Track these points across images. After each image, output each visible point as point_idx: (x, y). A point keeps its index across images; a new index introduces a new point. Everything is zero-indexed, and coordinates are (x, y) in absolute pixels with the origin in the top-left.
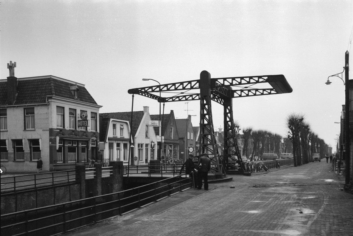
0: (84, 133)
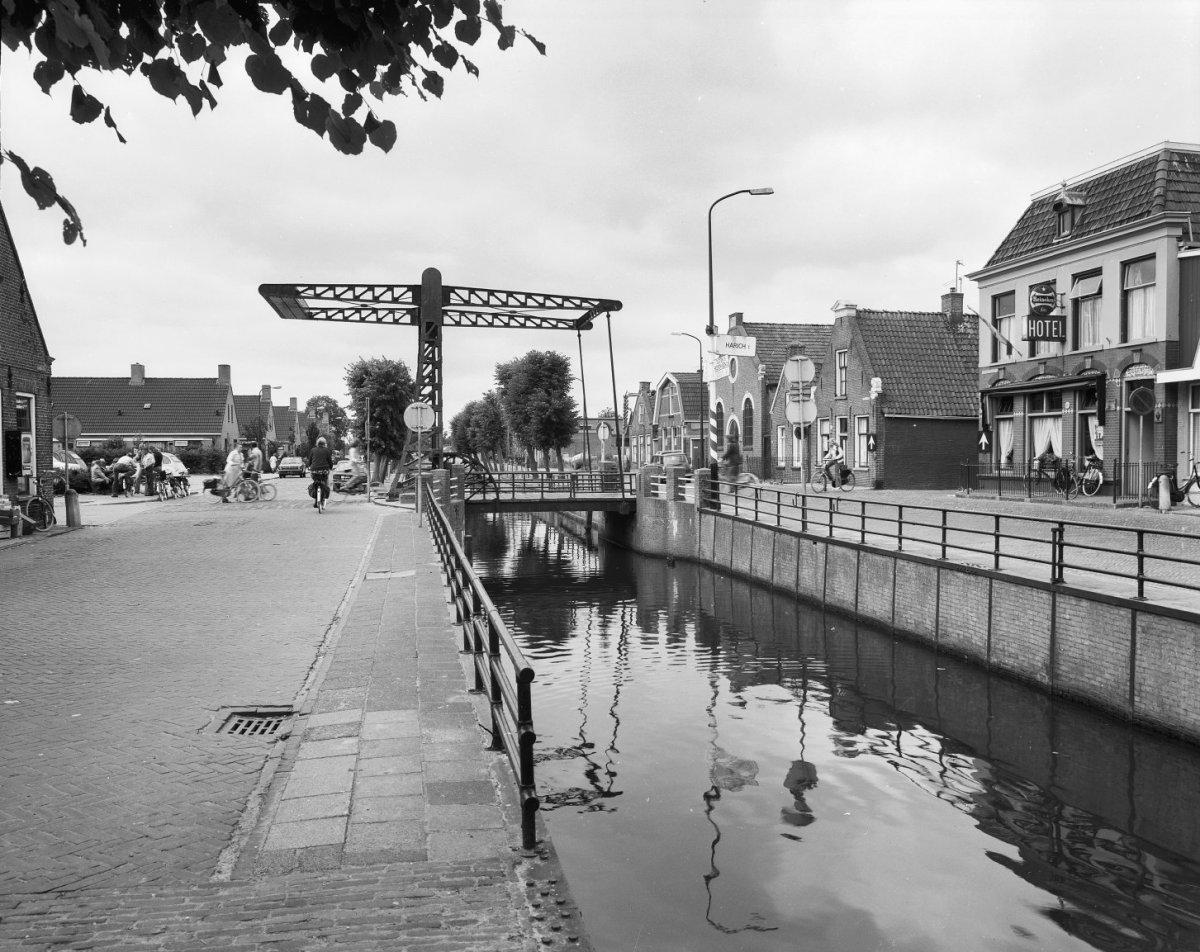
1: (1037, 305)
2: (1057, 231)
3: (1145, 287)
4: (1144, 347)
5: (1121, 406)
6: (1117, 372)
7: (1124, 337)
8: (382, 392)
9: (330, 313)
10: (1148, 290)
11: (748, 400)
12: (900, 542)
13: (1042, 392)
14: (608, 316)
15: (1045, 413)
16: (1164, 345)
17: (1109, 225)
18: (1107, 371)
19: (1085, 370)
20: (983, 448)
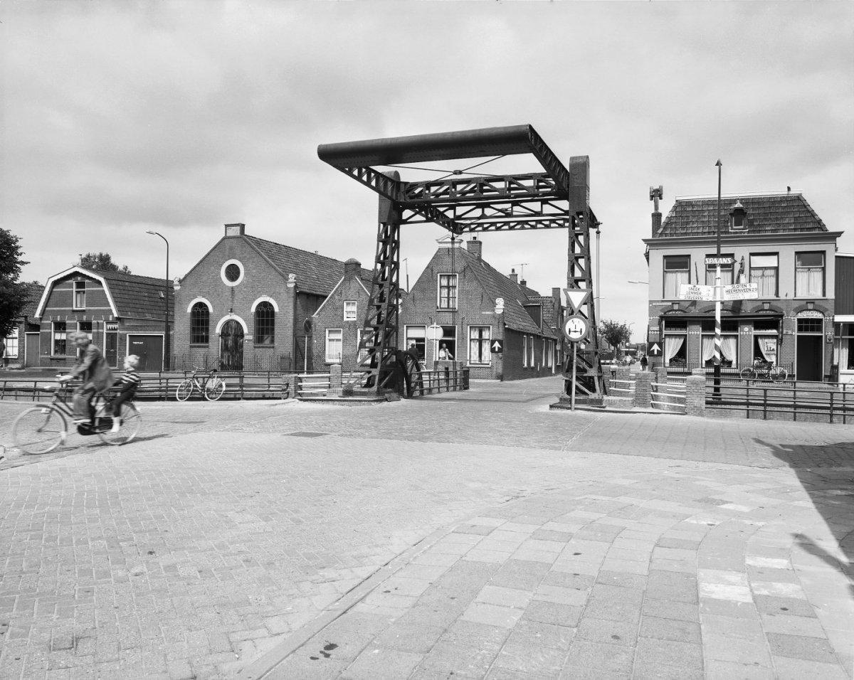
0: (807, 303)
16: (732, 302)
18: (784, 312)
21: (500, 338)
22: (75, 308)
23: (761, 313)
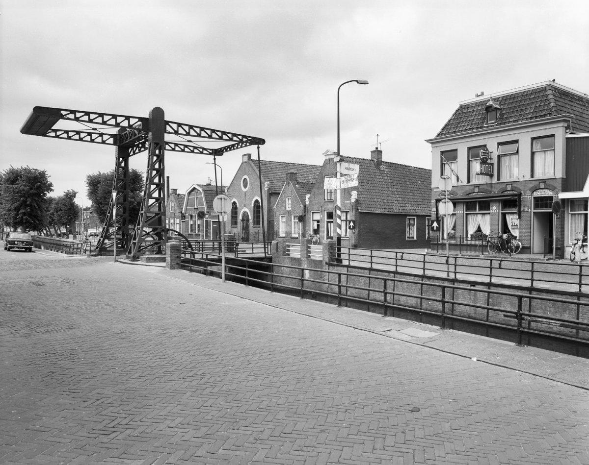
0: (507, 185)
1: (483, 157)
2: (484, 119)
3: (545, 151)
4: (547, 181)
5: (531, 209)
6: (529, 192)
7: (532, 176)
8: (31, 189)
9: (58, 133)
10: (547, 152)
11: (234, 203)
12: (580, 287)
13: (476, 201)
14: (258, 148)
15: (477, 212)
16: (561, 180)
17: (522, 119)
18: (522, 192)
19: (507, 191)
20: (435, 229)
21: (354, 219)
22: (195, 207)
23: (506, 193)
